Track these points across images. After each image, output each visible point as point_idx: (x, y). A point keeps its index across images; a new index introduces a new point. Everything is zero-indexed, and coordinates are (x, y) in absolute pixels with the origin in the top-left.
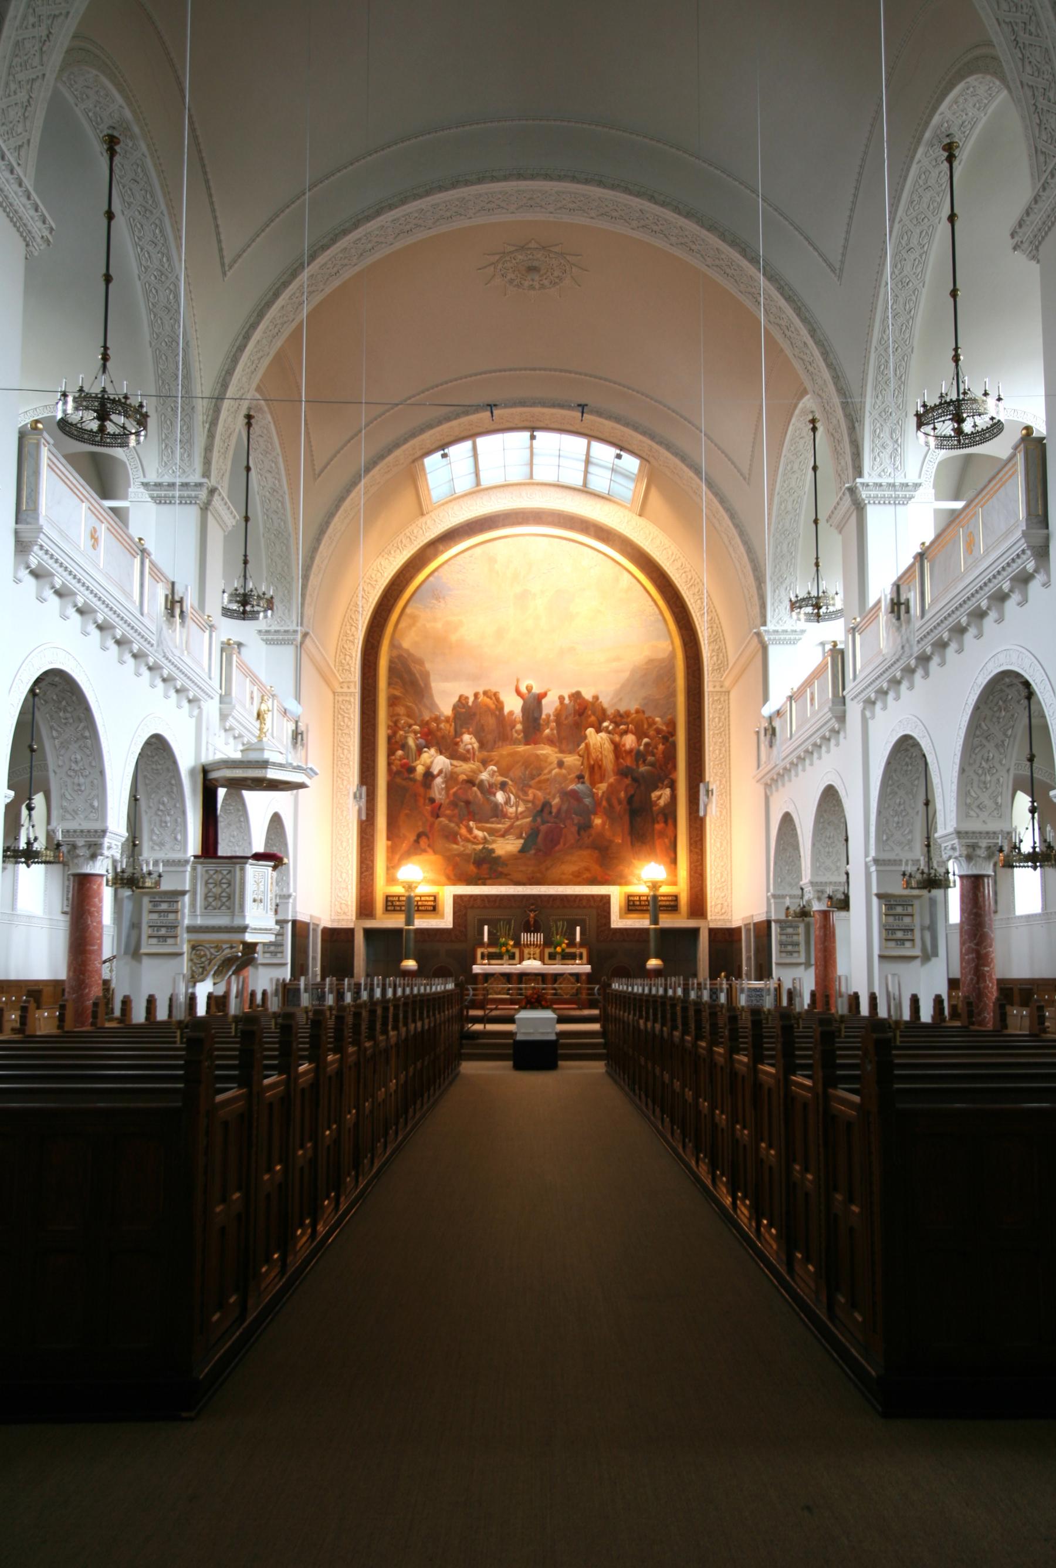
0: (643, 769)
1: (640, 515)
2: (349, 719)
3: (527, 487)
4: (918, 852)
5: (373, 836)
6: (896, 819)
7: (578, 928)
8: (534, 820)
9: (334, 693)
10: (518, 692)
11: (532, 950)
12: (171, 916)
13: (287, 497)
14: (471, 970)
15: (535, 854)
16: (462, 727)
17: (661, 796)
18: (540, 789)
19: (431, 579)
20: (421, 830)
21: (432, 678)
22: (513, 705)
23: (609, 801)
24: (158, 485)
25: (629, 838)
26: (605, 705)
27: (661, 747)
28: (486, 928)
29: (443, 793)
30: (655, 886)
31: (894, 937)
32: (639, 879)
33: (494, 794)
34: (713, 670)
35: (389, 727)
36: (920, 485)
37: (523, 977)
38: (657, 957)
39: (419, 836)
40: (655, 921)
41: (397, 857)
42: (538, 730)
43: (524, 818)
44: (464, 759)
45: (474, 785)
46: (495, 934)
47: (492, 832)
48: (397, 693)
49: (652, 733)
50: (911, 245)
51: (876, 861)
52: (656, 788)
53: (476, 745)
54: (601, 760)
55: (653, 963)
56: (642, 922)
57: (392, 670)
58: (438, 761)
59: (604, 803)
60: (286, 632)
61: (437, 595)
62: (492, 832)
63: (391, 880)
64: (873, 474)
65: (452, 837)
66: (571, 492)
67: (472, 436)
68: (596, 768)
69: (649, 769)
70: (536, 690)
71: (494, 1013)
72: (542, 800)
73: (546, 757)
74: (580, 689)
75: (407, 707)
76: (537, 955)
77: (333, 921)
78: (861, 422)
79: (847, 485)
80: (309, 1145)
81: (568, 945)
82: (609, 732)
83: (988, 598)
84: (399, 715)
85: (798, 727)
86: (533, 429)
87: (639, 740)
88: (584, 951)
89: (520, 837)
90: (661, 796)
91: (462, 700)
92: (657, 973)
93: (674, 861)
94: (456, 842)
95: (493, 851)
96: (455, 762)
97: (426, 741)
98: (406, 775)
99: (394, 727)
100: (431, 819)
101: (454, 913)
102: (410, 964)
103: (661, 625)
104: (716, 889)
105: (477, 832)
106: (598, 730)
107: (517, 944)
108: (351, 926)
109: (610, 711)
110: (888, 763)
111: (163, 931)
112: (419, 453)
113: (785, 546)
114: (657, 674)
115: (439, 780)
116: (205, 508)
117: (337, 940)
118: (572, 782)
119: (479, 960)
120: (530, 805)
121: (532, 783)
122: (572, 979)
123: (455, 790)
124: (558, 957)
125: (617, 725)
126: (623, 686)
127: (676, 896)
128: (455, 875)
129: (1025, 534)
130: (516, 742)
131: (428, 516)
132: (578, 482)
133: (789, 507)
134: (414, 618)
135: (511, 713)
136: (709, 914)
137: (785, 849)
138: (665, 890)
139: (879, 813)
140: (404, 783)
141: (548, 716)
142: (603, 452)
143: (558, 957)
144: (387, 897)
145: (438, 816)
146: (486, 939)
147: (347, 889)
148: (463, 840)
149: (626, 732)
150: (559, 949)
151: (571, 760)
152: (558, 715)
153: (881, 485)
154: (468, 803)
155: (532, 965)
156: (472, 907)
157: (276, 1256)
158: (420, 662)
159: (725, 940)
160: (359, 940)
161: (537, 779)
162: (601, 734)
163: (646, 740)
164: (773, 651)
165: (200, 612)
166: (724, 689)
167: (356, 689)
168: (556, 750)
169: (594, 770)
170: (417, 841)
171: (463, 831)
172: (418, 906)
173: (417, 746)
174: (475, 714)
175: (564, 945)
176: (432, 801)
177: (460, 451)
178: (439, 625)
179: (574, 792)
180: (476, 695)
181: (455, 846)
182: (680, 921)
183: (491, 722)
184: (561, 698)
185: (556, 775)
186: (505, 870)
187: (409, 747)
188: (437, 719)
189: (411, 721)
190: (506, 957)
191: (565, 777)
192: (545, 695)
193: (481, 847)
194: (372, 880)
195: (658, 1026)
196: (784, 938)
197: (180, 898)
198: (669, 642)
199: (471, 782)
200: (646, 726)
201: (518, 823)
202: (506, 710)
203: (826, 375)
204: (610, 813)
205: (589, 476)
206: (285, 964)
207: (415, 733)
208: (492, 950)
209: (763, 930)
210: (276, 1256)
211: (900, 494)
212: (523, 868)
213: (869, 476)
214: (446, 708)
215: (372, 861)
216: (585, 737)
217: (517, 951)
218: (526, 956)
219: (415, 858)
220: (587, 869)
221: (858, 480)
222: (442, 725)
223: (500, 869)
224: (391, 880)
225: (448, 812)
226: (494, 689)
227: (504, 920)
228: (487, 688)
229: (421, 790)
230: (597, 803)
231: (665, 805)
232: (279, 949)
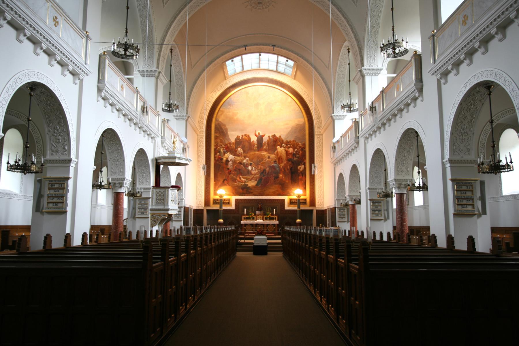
0: (295, 159)
4: (382, 186)
8: (261, 175)
10: (256, 135)
11: (260, 216)
12: (145, 206)
17: (301, 168)
21: (229, 130)
22: (254, 139)
23: (284, 169)
24: (143, 71)
26: (283, 139)
27: (301, 152)
30: (299, 196)
32: (294, 194)
35: (215, 146)
37: (257, 225)
39: (224, 180)
40: (299, 207)
44: (239, 156)
47: (247, 179)
48: (217, 135)
49: (298, 147)
51: (369, 189)
52: (299, 165)
53: (242, 152)
55: (298, 221)
56: (295, 208)
57: (216, 128)
58: (231, 157)
59: (283, 170)
60: (151, 71)
61: (230, 104)
62: (247, 179)
65: (234, 180)
67: (241, 55)
69: (296, 159)
70: (261, 134)
71: (248, 237)
78: (363, 50)
81: (271, 215)
85: (440, 55)
87: (294, 149)
88: (276, 217)
89: (256, 181)
90: (301, 168)
91: (238, 137)
92: (300, 224)
95: (247, 185)
99: (216, 146)
102: (221, 221)
103: (301, 114)
106: (281, 147)
107: (255, 214)
108: (202, 208)
109: (285, 141)
110: (373, 157)
114: (300, 129)
115: (230, 163)
116: (157, 78)
117: (198, 213)
125: (287, 145)
126: (289, 133)
129: (415, 85)
130: (255, 150)
132: (275, 69)
134: (223, 112)
135: (253, 141)
138: (302, 197)
139: (370, 173)
142: (282, 59)
149: (290, 147)
151: (272, 156)
152: (268, 142)
154: (240, 170)
155: (260, 221)
158: (225, 125)
159: (322, 213)
164: (336, 122)
167: (204, 134)
169: (279, 159)
170: (223, 182)
171: (238, 179)
176: (228, 169)
177: (237, 59)
178: (231, 114)
180: (242, 136)
182: (307, 207)
183: (247, 144)
184: (269, 137)
186: (251, 191)
188: (230, 143)
191: (270, 162)
192: (264, 136)
199: (240, 163)
202: (252, 140)
203: (352, 35)
204: (284, 173)
205: (279, 65)
206: (148, 217)
207: (223, 148)
209: (333, 210)
211: (376, 72)
213: (366, 66)
214: (233, 140)
216: (277, 149)
217: (255, 217)
219: (223, 187)
220: (277, 191)
224: (215, 194)
226: (248, 134)
229: (225, 166)
230: (281, 170)
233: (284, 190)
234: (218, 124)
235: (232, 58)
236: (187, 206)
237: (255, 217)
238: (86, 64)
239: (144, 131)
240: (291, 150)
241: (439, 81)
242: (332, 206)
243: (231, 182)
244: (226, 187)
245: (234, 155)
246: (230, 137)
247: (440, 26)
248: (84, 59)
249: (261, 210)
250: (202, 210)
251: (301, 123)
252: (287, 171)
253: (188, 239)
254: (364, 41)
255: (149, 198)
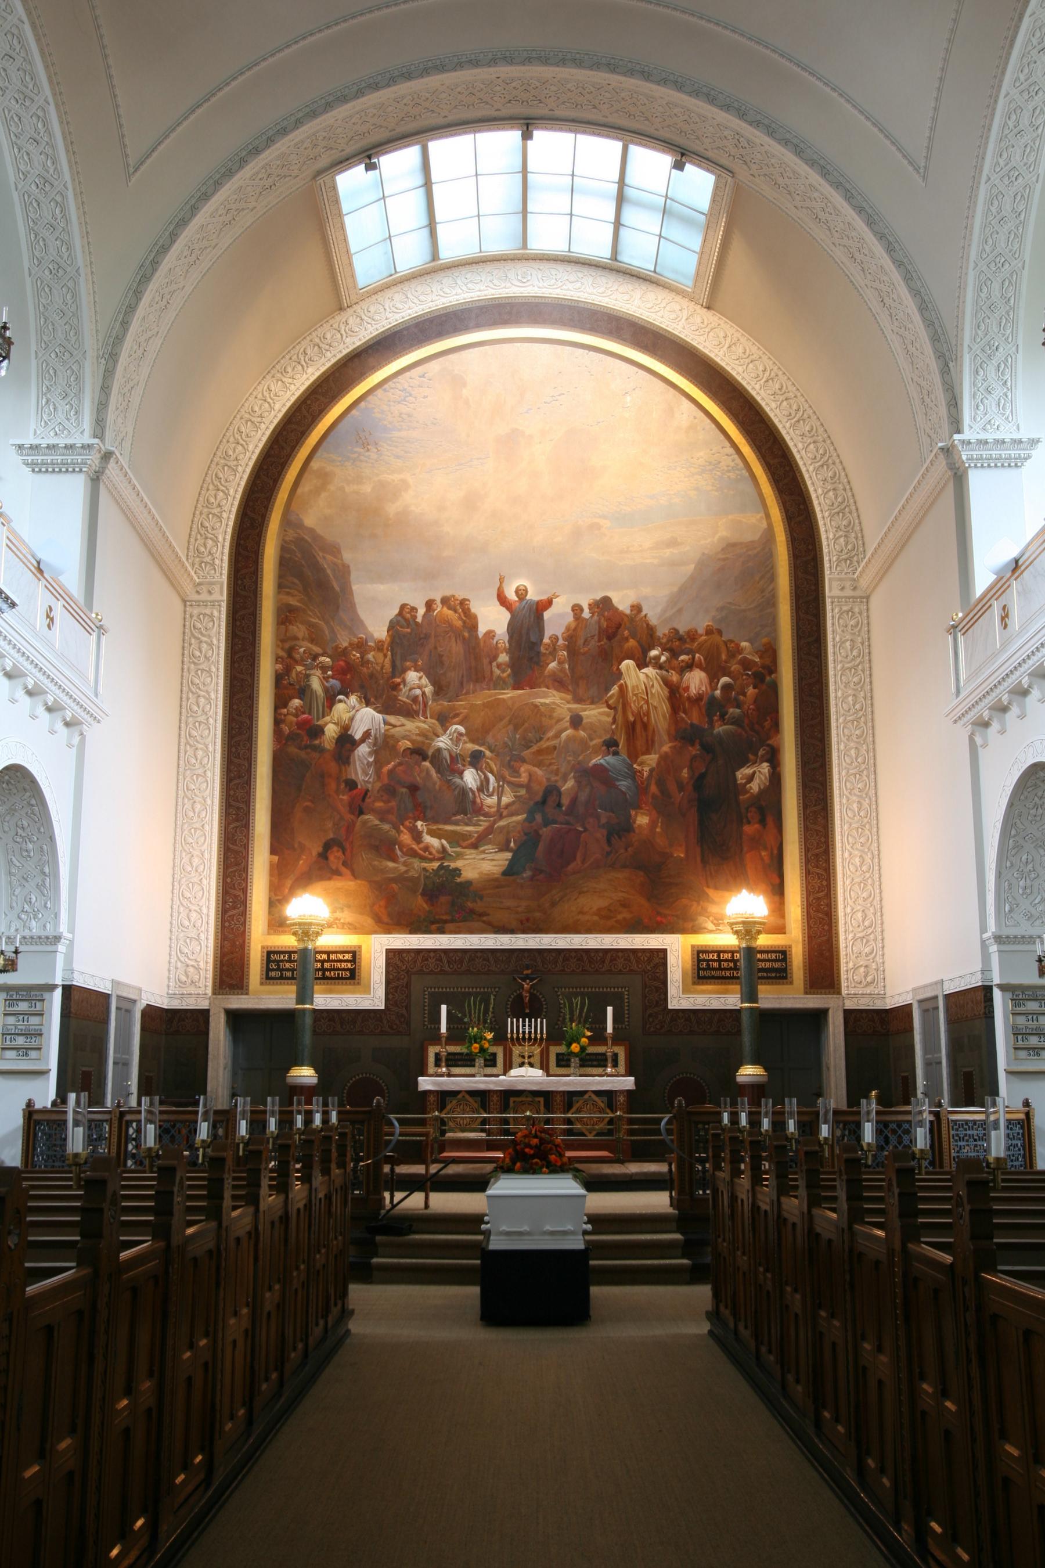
0: (720, 729)
1: (708, 308)
2: (210, 645)
3: (519, 265)
5: (246, 847)
6: (1022, 883)
7: (610, 1010)
8: (530, 819)
9: (184, 601)
10: (502, 600)
11: (526, 1049)
12: (34, 1020)
13: (70, 194)
14: (416, 1083)
15: (532, 879)
16: (404, 659)
17: (754, 776)
18: (539, 765)
19: (354, 412)
20: (331, 836)
21: (353, 576)
22: (493, 620)
23: (661, 783)
24: (35, 448)
25: (698, 850)
26: (653, 621)
27: (751, 691)
28: (444, 1008)
29: (371, 771)
30: (748, 929)
31: (1026, 1044)
32: (718, 921)
33: (461, 774)
34: (839, 561)
35: (278, 659)
36: (1038, 441)
37: (509, 1097)
38: (755, 1062)
39: (327, 846)
40: (751, 995)
41: (289, 883)
42: (538, 663)
43: (512, 815)
44: (409, 713)
45: (424, 759)
46: (461, 1020)
47: (456, 839)
48: (293, 602)
49: (735, 667)
50: (1021, 127)
51: (998, 939)
52: (743, 763)
53: (429, 690)
54: (648, 714)
55: (749, 1072)
56: (730, 999)
57: (284, 563)
58: (366, 719)
59: (654, 789)
60: (70, 447)
61: (364, 439)
62: (456, 839)
63: (277, 923)
64: (975, 427)
65: (386, 848)
66: (593, 272)
67: (417, 131)
68: (639, 727)
69: (731, 723)
70: (533, 596)
71: (453, 1169)
72: (545, 783)
73: (551, 709)
74: (610, 594)
75: (311, 626)
76: (536, 1060)
77: (171, 996)
78: (958, 359)
79: (940, 445)
80: (203, 1342)
81: (593, 1041)
82: (660, 667)
83: (1029, 675)
84: (296, 638)
85: (968, 681)
86: (527, 126)
87: (713, 678)
88: (621, 1051)
89: (505, 848)
90: (754, 776)
91: (406, 612)
92: (756, 1091)
93: (777, 891)
94: (394, 859)
95: (457, 872)
96: (392, 719)
97: (342, 682)
98: (306, 741)
99: (287, 658)
100: (350, 817)
101: (388, 982)
102: (305, 1074)
103: (748, 487)
104: (855, 939)
105: (428, 839)
106: (641, 665)
107: (501, 1038)
108: (204, 1005)
109: (662, 631)
110: (1011, 805)
111: (20, 1041)
112: (324, 162)
113: (996, 286)
114: (744, 566)
115: (363, 750)
116: (96, 479)
117: (173, 1034)
118: (596, 752)
119: (431, 1069)
120: (523, 792)
121: (526, 753)
122: (601, 1102)
123: (390, 766)
124: (574, 1061)
125: (674, 654)
126: (683, 589)
127: (784, 953)
128: (389, 915)
130: (499, 684)
131: (350, 311)
132: (602, 251)
133: (1007, 207)
134: (325, 477)
135: (490, 634)
136: (844, 984)
137: (1018, 847)
138: (764, 941)
139: (999, 875)
140: (303, 754)
141: (555, 639)
142: (651, 165)
143: (574, 1061)
144: (269, 953)
145: (361, 812)
146: (443, 1029)
147: (198, 939)
148: (404, 854)
149: (690, 666)
150: (575, 1048)
151: (595, 714)
152: (571, 636)
153: (986, 442)
154: (414, 789)
155: (527, 1076)
156: (420, 972)
157: (140, 1523)
158: (334, 550)
159: (880, 1034)
160: (219, 1033)
161: (535, 748)
162: (645, 670)
163: (725, 680)
164: (978, 482)
165: (85, 609)
166: (858, 593)
167: (221, 595)
168: (569, 697)
169: (635, 730)
170: (324, 856)
171: (406, 838)
172: (324, 970)
173: (326, 690)
174: (427, 637)
175: (584, 1041)
176: (352, 785)
177: (399, 163)
178: (367, 488)
179: (599, 769)
180: (429, 604)
181: (391, 864)
182: (788, 997)
183: (456, 649)
184: (577, 609)
185: (569, 739)
186: (479, 906)
187: (312, 692)
188: (361, 646)
189: (317, 649)
190: (479, 1062)
191: (584, 744)
192: (549, 603)
193: (436, 865)
194: (244, 924)
195: (767, 1192)
196: (1021, 1020)
197: (46, 995)
198: (762, 514)
199: (419, 752)
200: (724, 657)
201: (502, 823)
202: (482, 630)
203: (910, 304)
204: (663, 807)
205: (623, 232)
206: (45, 1073)
207: (324, 668)
208: (452, 1049)
209: (969, 1010)
210: (140, 1523)
212: (510, 903)
213: (970, 432)
214: (377, 626)
215: (245, 891)
216: (619, 674)
217: (499, 1051)
218: (516, 1060)
219: (320, 886)
220: (625, 904)
221: (956, 437)
222: (370, 656)
223: (469, 904)
224: (277, 923)
225: (379, 804)
226: (460, 595)
227: (476, 995)
228: (448, 593)
229: (333, 767)
230: (641, 789)
231: (761, 792)
232: (34, 1042)
233: (663, 900)
234: (299, 541)
235: (368, 155)
236: (92, 975)
237: (499, 1051)
238: (96, 695)
239: (67, 724)
240: (696, 681)
241: (971, 740)
242: (962, 975)
243: (364, 859)
244: (337, 883)
245: (385, 710)
246: (363, 613)
247: (973, 601)
248: (92, 684)
249: (534, 1014)
250: (205, 1014)
251: (750, 537)
252: (678, 797)
253: (96, 1181)
254: (959, 328)
255: (52, 988)
